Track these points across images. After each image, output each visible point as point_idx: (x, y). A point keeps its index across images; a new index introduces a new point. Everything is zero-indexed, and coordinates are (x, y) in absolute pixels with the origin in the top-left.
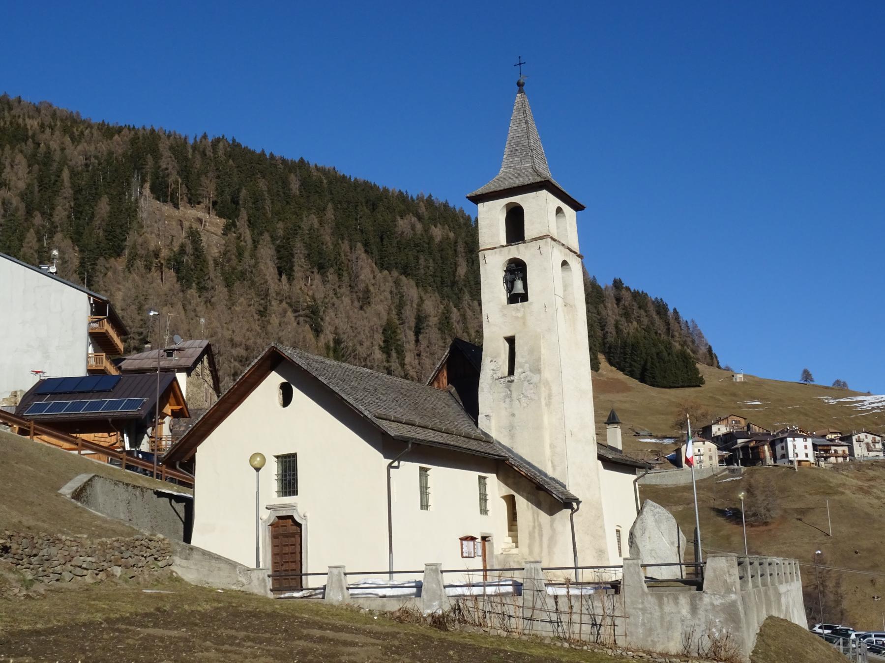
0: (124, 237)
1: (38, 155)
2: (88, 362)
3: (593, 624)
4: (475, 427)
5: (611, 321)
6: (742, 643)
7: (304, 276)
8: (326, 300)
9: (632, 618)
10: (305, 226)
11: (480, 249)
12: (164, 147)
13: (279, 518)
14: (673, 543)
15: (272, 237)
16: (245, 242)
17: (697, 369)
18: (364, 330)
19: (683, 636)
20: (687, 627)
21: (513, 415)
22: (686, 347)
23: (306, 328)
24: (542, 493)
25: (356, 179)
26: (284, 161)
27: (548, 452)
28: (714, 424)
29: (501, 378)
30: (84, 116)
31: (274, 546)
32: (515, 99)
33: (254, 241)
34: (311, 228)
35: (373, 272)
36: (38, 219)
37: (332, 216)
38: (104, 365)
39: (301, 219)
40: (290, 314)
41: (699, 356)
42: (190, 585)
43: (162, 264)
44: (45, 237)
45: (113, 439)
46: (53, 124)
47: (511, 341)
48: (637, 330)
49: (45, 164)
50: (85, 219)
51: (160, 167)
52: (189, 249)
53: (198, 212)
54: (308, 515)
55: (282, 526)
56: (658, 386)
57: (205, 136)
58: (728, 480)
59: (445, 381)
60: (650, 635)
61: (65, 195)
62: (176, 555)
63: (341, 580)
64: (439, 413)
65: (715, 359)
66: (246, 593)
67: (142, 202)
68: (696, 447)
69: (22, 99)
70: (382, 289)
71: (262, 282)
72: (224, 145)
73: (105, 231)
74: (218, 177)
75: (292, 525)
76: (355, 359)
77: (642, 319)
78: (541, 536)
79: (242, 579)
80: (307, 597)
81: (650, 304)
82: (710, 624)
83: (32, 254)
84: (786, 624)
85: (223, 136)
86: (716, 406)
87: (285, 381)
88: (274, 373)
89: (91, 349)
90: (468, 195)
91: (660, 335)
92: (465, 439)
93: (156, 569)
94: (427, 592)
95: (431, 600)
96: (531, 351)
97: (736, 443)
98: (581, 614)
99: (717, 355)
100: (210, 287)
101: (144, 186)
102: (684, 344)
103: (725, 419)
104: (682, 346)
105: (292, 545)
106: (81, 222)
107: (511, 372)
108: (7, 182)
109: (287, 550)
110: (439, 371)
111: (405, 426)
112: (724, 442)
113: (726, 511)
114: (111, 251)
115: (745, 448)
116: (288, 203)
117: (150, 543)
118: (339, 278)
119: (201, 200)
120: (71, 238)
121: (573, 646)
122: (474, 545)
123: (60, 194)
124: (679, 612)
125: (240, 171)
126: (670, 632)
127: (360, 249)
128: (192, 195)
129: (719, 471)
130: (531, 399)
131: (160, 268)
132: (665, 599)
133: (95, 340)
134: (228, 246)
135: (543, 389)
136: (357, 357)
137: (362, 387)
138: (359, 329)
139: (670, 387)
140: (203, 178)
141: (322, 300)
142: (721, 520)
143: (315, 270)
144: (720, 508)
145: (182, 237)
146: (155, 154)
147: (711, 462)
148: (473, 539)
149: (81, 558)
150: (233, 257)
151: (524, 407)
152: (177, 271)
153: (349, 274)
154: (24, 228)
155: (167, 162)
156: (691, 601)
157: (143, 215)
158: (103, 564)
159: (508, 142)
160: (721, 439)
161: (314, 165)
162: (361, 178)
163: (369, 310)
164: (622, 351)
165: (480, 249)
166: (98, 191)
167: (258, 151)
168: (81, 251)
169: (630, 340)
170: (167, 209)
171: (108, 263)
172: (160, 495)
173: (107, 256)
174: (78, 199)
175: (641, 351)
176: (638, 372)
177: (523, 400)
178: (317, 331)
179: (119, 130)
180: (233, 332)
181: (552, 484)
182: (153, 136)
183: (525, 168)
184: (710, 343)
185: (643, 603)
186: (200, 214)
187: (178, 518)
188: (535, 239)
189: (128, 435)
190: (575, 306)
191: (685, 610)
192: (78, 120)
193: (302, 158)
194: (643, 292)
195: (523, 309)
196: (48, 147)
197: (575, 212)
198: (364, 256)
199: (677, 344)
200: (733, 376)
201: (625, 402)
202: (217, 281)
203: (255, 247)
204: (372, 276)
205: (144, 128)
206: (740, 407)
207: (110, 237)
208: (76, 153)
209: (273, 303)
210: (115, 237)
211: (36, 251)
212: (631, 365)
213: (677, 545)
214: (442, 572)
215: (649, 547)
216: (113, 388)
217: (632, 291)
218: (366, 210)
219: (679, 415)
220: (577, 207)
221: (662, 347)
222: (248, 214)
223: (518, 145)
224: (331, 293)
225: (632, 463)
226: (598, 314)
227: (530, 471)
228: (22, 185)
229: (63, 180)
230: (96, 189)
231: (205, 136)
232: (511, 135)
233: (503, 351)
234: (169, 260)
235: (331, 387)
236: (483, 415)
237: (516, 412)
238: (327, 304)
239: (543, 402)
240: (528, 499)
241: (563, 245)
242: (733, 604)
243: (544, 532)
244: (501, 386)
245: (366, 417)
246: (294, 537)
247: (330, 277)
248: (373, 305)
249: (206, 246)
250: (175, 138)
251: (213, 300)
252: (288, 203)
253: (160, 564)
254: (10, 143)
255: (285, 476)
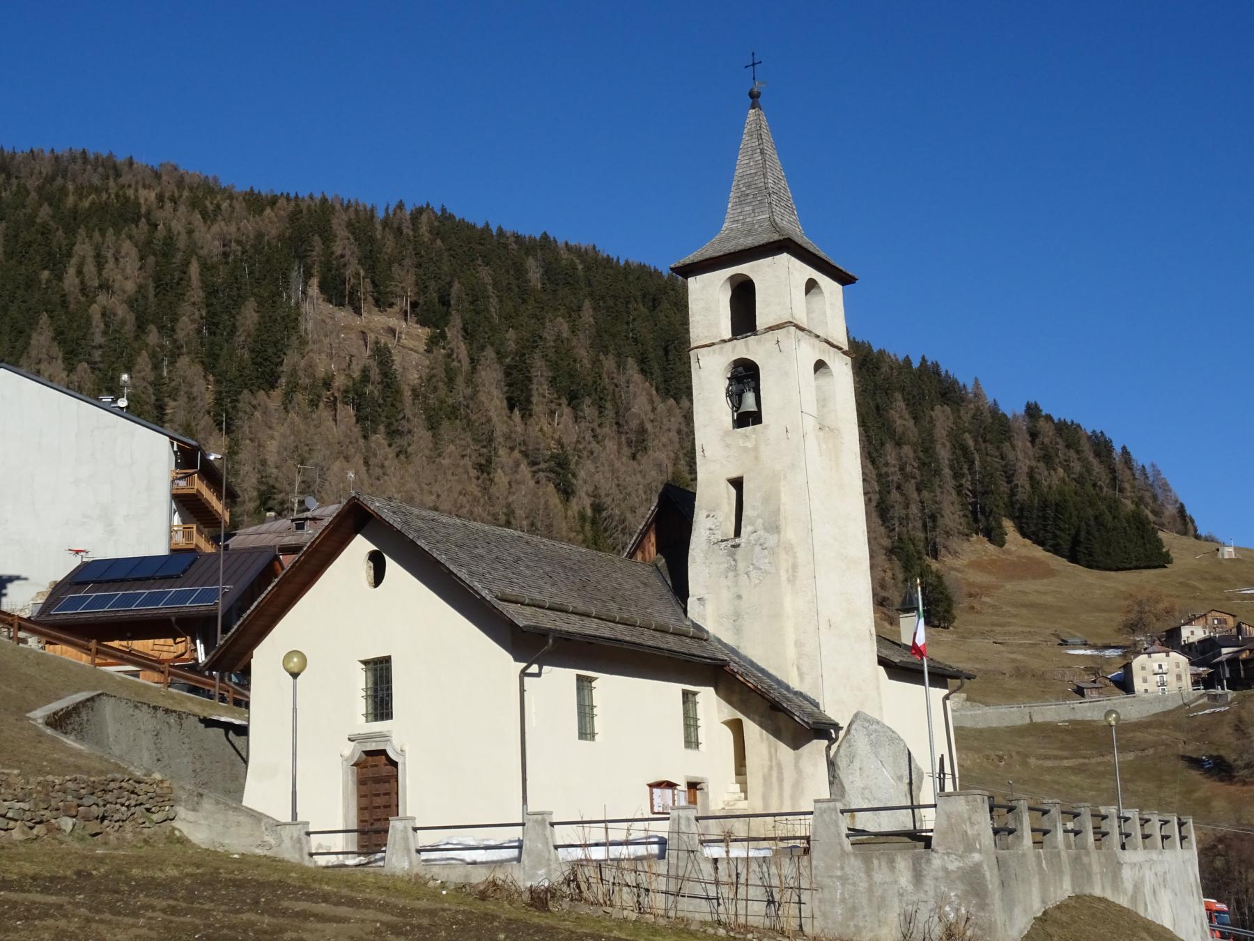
0: (280, 360)
1: (155, 242)
2: (171, 538)
3: (768, 901)
4: (683, 615)
5: (1023, 467)
6: (990, 928)
7: (547, 411)
8: (581, 447)
9: (826, 891)
10: (549, 335)
11: (692, 346)
12: (338, 224)
13: (369, 753)
14: (900, 778)
15: (498, 353)
16: (460, 361)
17: (1159, 541)
18: (637, 490)
19: (902, 918)
20: (907, 905)
21: (739, 597)
22: (1142, 506)
23: (548, 489)
24: (781, 715)
25: (627, 262)
26: (518, 239)
27: (791, 652)
28: (1184, 624)
29: (722, 541)
30: (224, 183)
31: (361, 796)
32: (746, 118)
33: (472, 360)
34: (558, 337)
35: (651, 401)
36: (153, 337)
37: (591, 319)
38: (194, 542)
39: (543, 324)
40: (524, 468)
41: (1165, 520)
42: (199, 848)
43: (336, 398)
44: (166, 363)
45: (180, 648)
46: (177, 195)
47: (737, 483)
48: (1063, 481)
49: (165, 255)
50: (222, 334)
51: (332, 253)
52: (375, 374)
53: (377, 320)
54: (406, 748)
55: (372, 766)
56: (1098, 568)
57: (401, 206)
58: (1207, 711)
59: (653, 550)
60: (853, 917)
61: (193, 300)
62: (180, 805)
63: (408, 838)
64: (623, 596)
65: (1190, 524)
66: (273, 859)
67: (306, 307)
68: (1155, 661)
69: (135, 160)
70: (665, 428)
71: (484, 420)
72: (429, 218)
73: (252, 351)
74: (419, 266)
75: (386, 765)
76: (624, 534)
77: (1072, 464)
78: (781, 780)
79: (270, 839)
80: (363, 864)
81: (1084, 441)
82: (942, 899)
83: (145, 387)
84: (1102, 906)
85: (428, 205)
86: (1190, 598)
87: (375, 548)
88: (359, 537)
89: (177, 519)
90: (672, 266)
91: (1101, 488)
92: (658, 634)
93: (147, 824)
94: (529, 855)
95: (534, 868)
96: (766, 500)
97: (1220, 654)
98: (747, 885)
99: (1194, 517)
100: (406, 429)
101: (310, 283)
102: (1139, 501)
103: (1202, 616)
104: (1137, 505)
105: (385, 794)
106: (217, 339)
107: (738, 533)
108: (110, 282)
109: (379, 801)
110: (644, 534)
111: (549, 612)
112: (1200, 653)
113: (1204, 761)
114: (261, 381)
115: (1233, 661)
116: (524, 301)
117: (137, 785)
118: (601, 412)
119: (393, 300)
120: (202, 362)
121: (732, 934)
122: (674, 795)
123: (186, 298)
124: (896, 882)
125: (451, 255)
126: (882, 912)
127: (632, 368)
128: (379, 293)
129: (1192, 698)
130: (766, 572)
131: (333, 404)
132: (875, 862)
133: (184, 505)
134: (433, 369)
135: (783, 556)
136: (627, 530)
137: (494, 556)
138: (629, 489)
139: (1118, 569)
140: (395, 268)
141: (573, 445)
142: (1195, 774)
143: (564, 401)
144: (1195, 756)
145: (364, 357)
146: (326, 234)
147: (1180, 684)
148: (670, 785)
149: (6, 803)
150: (441, 384)
151: (756, 586)
152: (358, 408)
153: (616, 405)
154: (134, 349)
155: (344, 245)
156: (914, 864)
157: (308, 325)
158: (42, 812)
159: (734, 183)
160: (1196, 647)
161: (564, 241)
162: (635, 259)
163: (646, 461)
164: (1040, 514)
165: (692, 346)
166: (242, 292)
167: (480, 225)
168: (218, 382)
169: (1053, 497)
170: (344, 316)
171: (256, 398)
172: (209, 723)
173: (254, 388)
174: (212, 304)
175: (1071, 514)
176: (1066, 546)
177: (754, 574)
178: (567, 492)
179: (273, 201)
180: (438, 496)
181: (797, 701)
182: (325, 209)
183: (759, 222)
184: (1182, 499)
185: (842, 868)
186: (394, 322)
187: (239, 758)
188: (771, 329)
189: (204, 642)
190: (838, 430)
191: (905, 879)
192: (216, 189)
193: (545, 233)
194: (1072, 422)
195: (754, 436)
196: (169, 230)
197: (840, 287)
198: (637, 377)
199: (1128, 502)
200: (1218, 550)
201: (1045, 593)
202: (416, 421)
203: (474, 370)
204: (649, 408)
205: (311, 197)
206: (1228, 599)
207: (259, 360)
208: (209, 236)
209: (501, 452)
210: (266, 360)
211: (151, 384)
212: (1055, 536)
213: (908, 781)
214: (552, 824)
215: (859, 783)
216: (184, 572)
217: (1056, 421)
218: (642, 308)
219: (1129, 612)
220: (844, 279)
221: (1103, 508)
222: (463, 319)
223: (749, 187)
224: (588, 435)
225: (940, 671)
226: (1002, 458)
227: (761, 681)
228: (130, 287)
229: (190, 278)
230: (239, 289)
231: (401, 206)
232: (739, 171)
233: (725, 501)
234: (346, 391)
235: (435, 555)
236: (695, 599)
237: (744, 593)
238: (580, 451)
239: (784, 576)
240: (761, 725)
241: (817, 336)
242: (976, 868)
243: (785, 776)
244: (722, 552)
245: (484, 598)
246: (389, 782)
247: (587, 411)
248: (650, 452)
249: (400, 370)
250: (356, 210)
251: (410, 450)
252: (524, 301)
253: (155, 817)
254: (115, 225)
255: (376, 691)
